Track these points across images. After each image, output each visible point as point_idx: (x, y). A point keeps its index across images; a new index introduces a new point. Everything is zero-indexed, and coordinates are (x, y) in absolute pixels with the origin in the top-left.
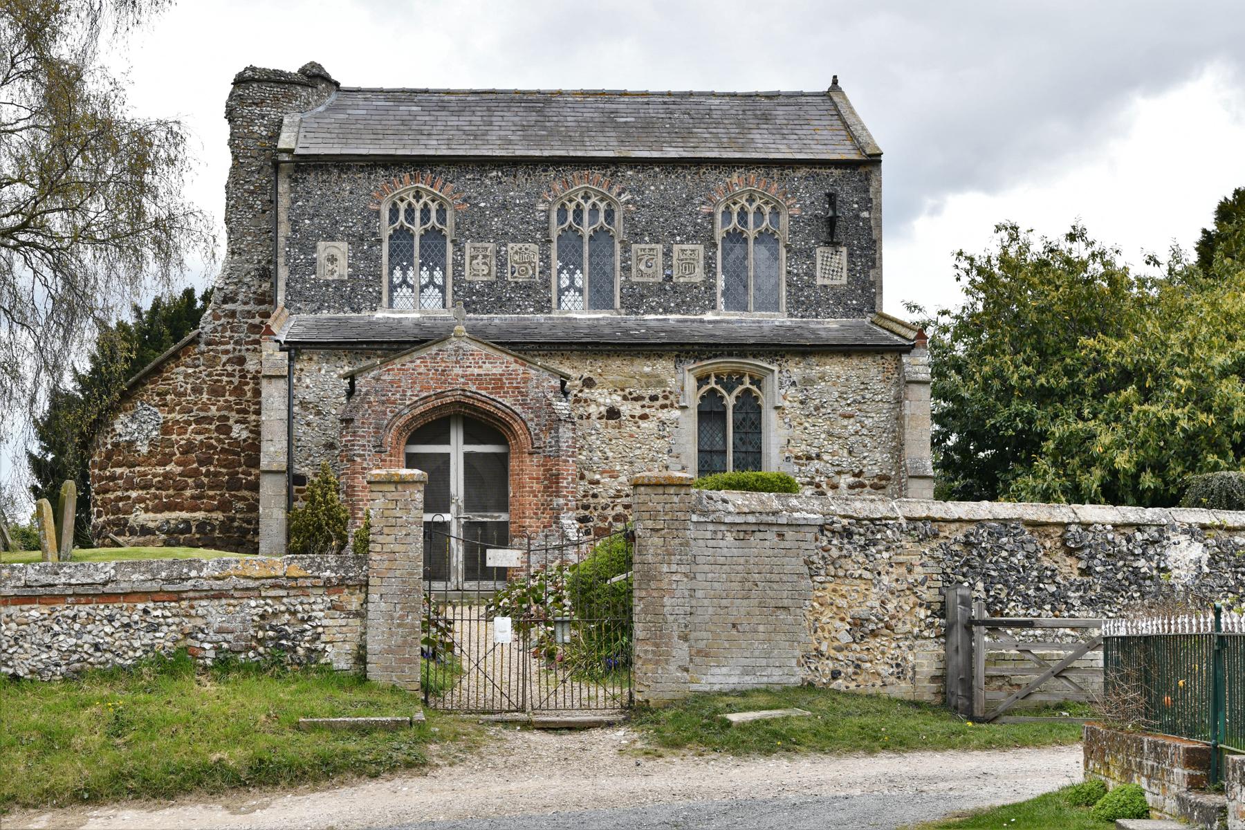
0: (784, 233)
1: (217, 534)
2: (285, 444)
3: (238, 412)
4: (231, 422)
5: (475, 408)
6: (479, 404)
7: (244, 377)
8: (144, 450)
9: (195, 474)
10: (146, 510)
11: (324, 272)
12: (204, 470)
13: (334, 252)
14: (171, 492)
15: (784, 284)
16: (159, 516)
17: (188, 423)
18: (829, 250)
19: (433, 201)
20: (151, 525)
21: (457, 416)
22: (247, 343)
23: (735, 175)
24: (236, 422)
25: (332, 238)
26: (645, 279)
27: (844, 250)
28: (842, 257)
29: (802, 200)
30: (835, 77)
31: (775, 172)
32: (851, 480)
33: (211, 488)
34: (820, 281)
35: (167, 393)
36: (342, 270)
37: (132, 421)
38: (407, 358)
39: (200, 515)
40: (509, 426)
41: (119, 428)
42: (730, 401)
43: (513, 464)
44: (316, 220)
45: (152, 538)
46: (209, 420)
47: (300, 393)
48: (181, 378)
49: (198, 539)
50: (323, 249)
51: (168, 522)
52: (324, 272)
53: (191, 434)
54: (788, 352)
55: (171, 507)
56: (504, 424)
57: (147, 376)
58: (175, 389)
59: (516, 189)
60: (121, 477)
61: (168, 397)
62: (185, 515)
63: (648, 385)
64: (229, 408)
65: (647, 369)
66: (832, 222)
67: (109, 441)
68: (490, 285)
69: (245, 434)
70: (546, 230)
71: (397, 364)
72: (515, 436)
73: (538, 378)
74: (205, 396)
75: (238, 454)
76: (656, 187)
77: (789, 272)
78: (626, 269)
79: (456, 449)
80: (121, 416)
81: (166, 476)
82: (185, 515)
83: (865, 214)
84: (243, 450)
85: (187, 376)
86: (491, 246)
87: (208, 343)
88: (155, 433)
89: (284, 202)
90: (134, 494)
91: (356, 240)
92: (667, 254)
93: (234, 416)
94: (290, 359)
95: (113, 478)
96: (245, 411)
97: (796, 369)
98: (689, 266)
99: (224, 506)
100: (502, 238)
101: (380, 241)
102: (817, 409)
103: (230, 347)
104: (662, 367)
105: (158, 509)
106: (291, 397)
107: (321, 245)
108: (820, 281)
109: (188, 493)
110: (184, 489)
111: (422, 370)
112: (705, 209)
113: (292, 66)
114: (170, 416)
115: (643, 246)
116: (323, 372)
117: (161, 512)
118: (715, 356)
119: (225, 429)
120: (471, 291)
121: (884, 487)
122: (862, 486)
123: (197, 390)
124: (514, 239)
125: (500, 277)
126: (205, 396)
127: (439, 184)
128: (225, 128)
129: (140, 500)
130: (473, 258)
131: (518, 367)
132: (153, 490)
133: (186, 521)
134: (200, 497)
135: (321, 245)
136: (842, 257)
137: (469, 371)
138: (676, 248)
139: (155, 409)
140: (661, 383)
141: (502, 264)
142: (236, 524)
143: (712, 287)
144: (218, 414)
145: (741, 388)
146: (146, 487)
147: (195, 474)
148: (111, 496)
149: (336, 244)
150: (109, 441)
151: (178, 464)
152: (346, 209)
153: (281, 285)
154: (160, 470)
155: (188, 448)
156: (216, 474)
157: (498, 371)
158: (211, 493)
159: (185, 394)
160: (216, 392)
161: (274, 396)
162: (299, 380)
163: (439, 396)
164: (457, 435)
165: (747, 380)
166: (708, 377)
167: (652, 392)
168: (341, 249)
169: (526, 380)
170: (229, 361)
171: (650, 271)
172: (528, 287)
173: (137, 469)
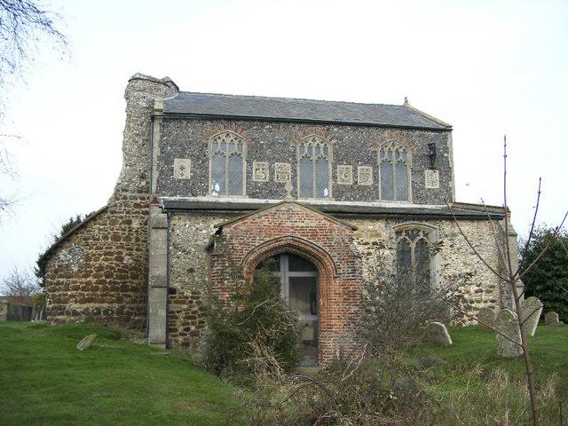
0: (410, 163)
1: (115, 316)
2: (165, 269)
3: (128, 249)
5: (299, 248)
7: (131, 231)
8: (75, 269)
10: (76, 302)
11: (177, 175)
12: (108, 280)
15: (410, 188)
17: (101, 255)
18: (431, 171)
19: (236, 139)
20: (79, 310)
21: (287, 253)
22: (133, 213)
23: (386, 133)
24: (127, 255)
25: (182, 157)
26: (345, 183)
27: (438, 171)
28: (436, 175)
29: (420, 142)
30: (406, 98)
31: (405, 132)
32: (477, 288)
33: (111, 290)
34: (427, 187)
35: (89, 239)
36: (188, 174)
38: (256, 216)
39: (105, 305)
40: (320, 260)
41: (62, 257)
42: (413, 245)
43: (323, 284)
44: (174, 147)
47: (174, 239)
50: (177, 163)
51: (87, 309)
52: (177, 175)
54: (443, 219)
55: (90, 300)
57: (72, 233)
58: (93, 237)
59: (280, 134)
62: (97, 305)
63: (372, 236)
64: (122, 247)
65: (370, 228)
66: (432, 157)
67: (56, 264)
68: (266, 184)
69: (131, 261)
70: (294, 157)
71: (249, 220)
72: (324, 266)
73: (338, 228)
76: (348, 135)
77: (413, 182)
78: (335, 178)
79: (285, 274)
80: (64, 251)
81: (89, 283)
82: (97, 305)
83: (446, 155)
86: (267, 163)
87: (112, 212)
89: (157, 137)
91: (195, 158)
92: (355, 170)
93: (125, 252)
94: (168, 218)
95: (58, 283)
96: (131, 249)
97: (447, 227)
98: (365, 175)
99: (119, 300)
100: (272, 160)
102: (458, 249)
104: (379, 226)
105: (83, 301)
106: (169, 241)
107: (176, 160)
108: (427, 187)
109: (99, 293)
111: (266, 223)
112: (372, 149)
113: (160, 77)
114: (90, 252)
115: (343, 166)
118: (406, 220)
119: (120, 259)
120: (256, 187)
121: (491, 292)
122: (481, 291)
123: (105, 238)
124: (278, 161)
125: (272, 180)
127: (240, 130)
128: (124, 103)
129: (72, 296)
131: (326, 222)
132: (80, 291)
133: (97, 309)
135: (176, 160)
136: (436, 175)
137: (296, 224)
138: (359, 168)
140: (378, 235)
141: (272, 173)
143: (376, 188)
144: (116, 251)
145: (419, 238)
146: (76, 288)
147: (104, 281)
148: (57, 293)
149: (185, 160)
150: (56, 264)
151: (95, 277)
153: (154, 181)
155: (100, 268)
157: (314, 225)
158: (112, 293)
159: (98, 240)
160: (116, 238)
161: (158, 237)
162: (173, 231)
163: (277, 240)
164: (284, 264)
165: (421, 233)
166: (401, 232)
167: (373, 240)
168: (187, 163)
169: (331, 231)
170: (123, 222)
171: (347, 179)
173: (71, 280)
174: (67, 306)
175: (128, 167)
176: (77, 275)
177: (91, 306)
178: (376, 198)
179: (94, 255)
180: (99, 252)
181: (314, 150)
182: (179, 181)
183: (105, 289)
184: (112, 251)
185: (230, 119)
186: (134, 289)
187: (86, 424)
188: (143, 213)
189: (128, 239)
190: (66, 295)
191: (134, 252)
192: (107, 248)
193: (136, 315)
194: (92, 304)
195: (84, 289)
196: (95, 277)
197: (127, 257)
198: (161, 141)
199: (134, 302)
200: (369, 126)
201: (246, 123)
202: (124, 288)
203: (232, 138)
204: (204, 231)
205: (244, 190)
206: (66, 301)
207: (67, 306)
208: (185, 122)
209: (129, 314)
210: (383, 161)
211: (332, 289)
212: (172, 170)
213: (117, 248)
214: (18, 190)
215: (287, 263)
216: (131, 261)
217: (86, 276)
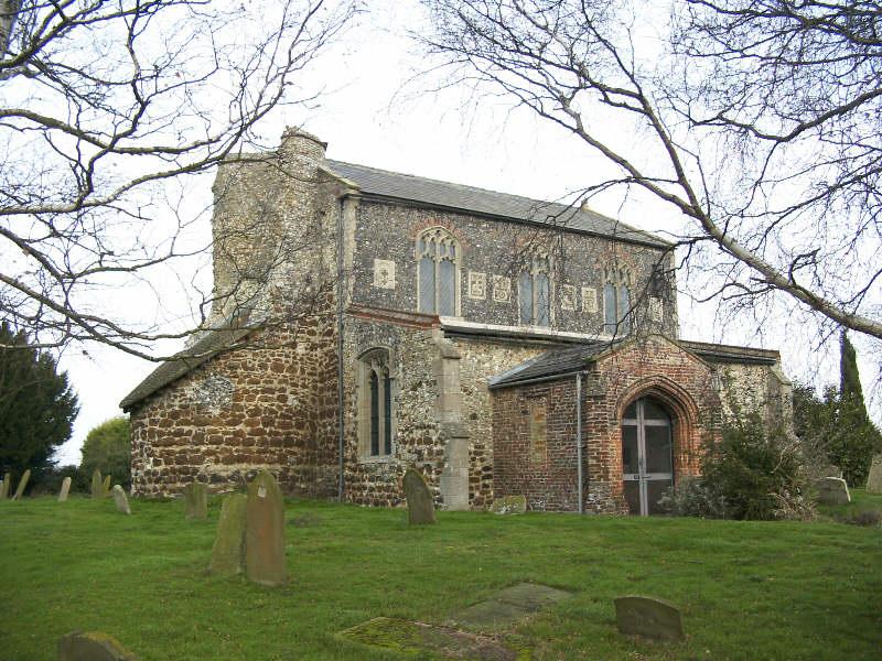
4: (287, 393)
6: (668, 388)
8: (216, 412)
10: (217, 462)
12: (268, 430)
13: (386, 267)
14: (241, 447)
17: (257, 392)
20: (224, 474)
35: (236, 367)
36: (391, 284)
37: (204, 388)
41: (189, 393)
46: (272, 391)
50: (379, 265)
51: (238, 472)
55: (240, 460)
56: (680, 405)
60: (189, 432)
61: (239, 371)
62: (253, 467)
64: (285, 381)
67: (177, 402)
74: (269, 371)
75: (290, 418)
80: (194, 384)
81: (237, 434)
82: (253, 467)
84: (294, 415)
86: (484, 275)
90: (203, 448)
93: (290, 389)
99: (282, 459)
105: (228, 461)
107: (377, 261)
109: (254, 448)
116: (468, 356)
119: (283, 399)
126: (269, 371)
129: (209, 453)
130: (473, 283)
132: (223, 445)
133: (253, 472)
139: (228, 380)
142: (290, 474)
144: (279, 386)
146: (218, 442)
147: (261, 432)
151: (248, 424)
152: (393, 236)
154: (230, 429)
155: (256, 412)
156: (277, 434)
158: (273, 449)
159: (253, 369)
160: (278, 368)
172: (505, 306)
173: (206, 428)
174: (202, 468)
176: (216, 421)
177: (244, 468)
178: (530, 321)
179: (246, 392)
180: (255, 387)
181: (438, 247)
182: (381, 290)
183: (263, 442)
184: (273, 386)
185: (442, 210)
186: (300, 444)
187: (184, 658)
188: (309, 333)
189: (292, 369)
190: (198, 450)
191: (299, 390)
192: (266, 382)
193: (302, 482)
194: (244, 465)
195: (229, 442)
197: (291, 397)
198: (357, 232)
199: (299, 462)
200: (592, 235)
201: (461, 218)
202: (288, 442)
203: (444, 237)
204: (487, 365)
205: (459, 308)
206: (200, 461)
207: (202, 468)
208: (386, 208)
209: (294, 479)
210: (424, 257)
211: (694, 437)
212: (372, 274)
213: (280, 382)
215: (642, 410)
216: (296, 402)
217: (234, 423)
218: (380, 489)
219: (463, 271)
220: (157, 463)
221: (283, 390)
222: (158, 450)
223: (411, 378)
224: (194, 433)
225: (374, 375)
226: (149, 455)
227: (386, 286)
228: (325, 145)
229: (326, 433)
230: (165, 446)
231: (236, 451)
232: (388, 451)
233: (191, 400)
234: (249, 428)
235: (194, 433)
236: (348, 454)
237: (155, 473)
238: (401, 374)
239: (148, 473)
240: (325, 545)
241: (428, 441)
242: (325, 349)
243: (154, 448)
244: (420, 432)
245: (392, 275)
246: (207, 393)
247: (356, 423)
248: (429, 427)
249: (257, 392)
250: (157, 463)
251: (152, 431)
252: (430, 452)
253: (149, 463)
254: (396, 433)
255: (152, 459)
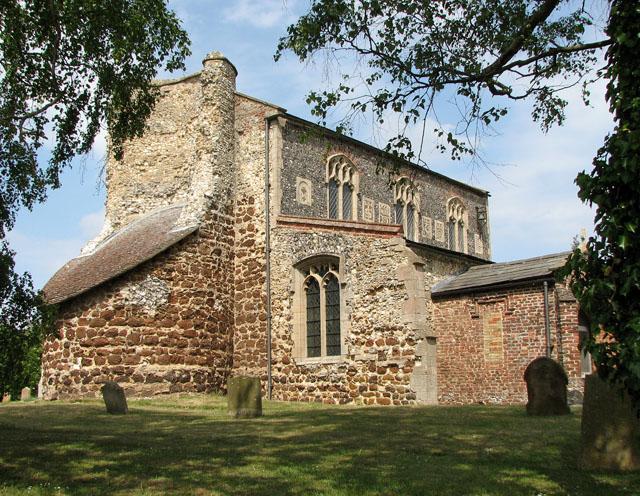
9: (192, 335)
10: (152, 362)
12: (199, 332)
16: (167, 367)
17: (189, 295)
20: (160, 374)
39: (196, 367)
45: (159, 384)
46: (203, 294)
48: (184, 260)
49: (195, 387)
51: (174, 371)
53: (191, 304)
60: (124, 333)
81: (172, 335)
82: (185, 366)
85: (188, 258)
86: (373, 201)
88: (164, 301)
90: (139, 349)
93: (216, 293)
99: (209, 363)
101: (403, 207)
103: (214, 241)
110: (185, 346)
114: (175, 289)
117: (167, 364)
129: (145, 354)
130: (366, 207)
132: (159, 346)
133: (187, 372)
134: (197, 353)
144: (208, 290)
147: (192, 335)
173: (141, 328)
175: (217, 177)
194: (179, 366)
196: (182, 328)
206: (136, 361)
214: (382, 121)
216: (220, 308)
218: (323, 389)
219: (359, 195)
220: (86, 363)
221: (211, 294)
222: (87, 351)
223: (368, 281)
224: (129, 333)
225: (312, 282)
226: (76, 355)
227: (305, 203)
228: (57, 185)
229: (246, 337)
230: (97, 346)
231: (171, 352)
232: (334, 348)
233: (127, 300)
234: (182, 331)
235: (129, 333)
236: (279, 356)
237: (83, 374)
238: (355, 280)
239: (74, 373)
240: (220, 435)
241: (392, 342)
242: (244, 259)
243: (83, 348)
244: (380, 334)
245: (309, 194)
246: (143, 294)
247: (291, 326)
248: (394, 329)
249: (189, 295)
250: (86, 363)
251: (81, 330)
252: (396, 351)
253: (75, 363)
254: (346, 329)
255: (80, 359)
